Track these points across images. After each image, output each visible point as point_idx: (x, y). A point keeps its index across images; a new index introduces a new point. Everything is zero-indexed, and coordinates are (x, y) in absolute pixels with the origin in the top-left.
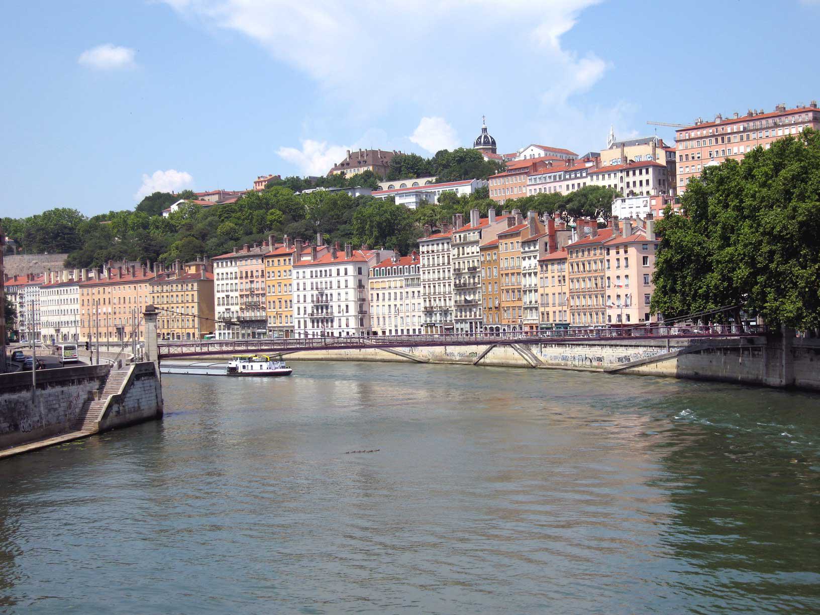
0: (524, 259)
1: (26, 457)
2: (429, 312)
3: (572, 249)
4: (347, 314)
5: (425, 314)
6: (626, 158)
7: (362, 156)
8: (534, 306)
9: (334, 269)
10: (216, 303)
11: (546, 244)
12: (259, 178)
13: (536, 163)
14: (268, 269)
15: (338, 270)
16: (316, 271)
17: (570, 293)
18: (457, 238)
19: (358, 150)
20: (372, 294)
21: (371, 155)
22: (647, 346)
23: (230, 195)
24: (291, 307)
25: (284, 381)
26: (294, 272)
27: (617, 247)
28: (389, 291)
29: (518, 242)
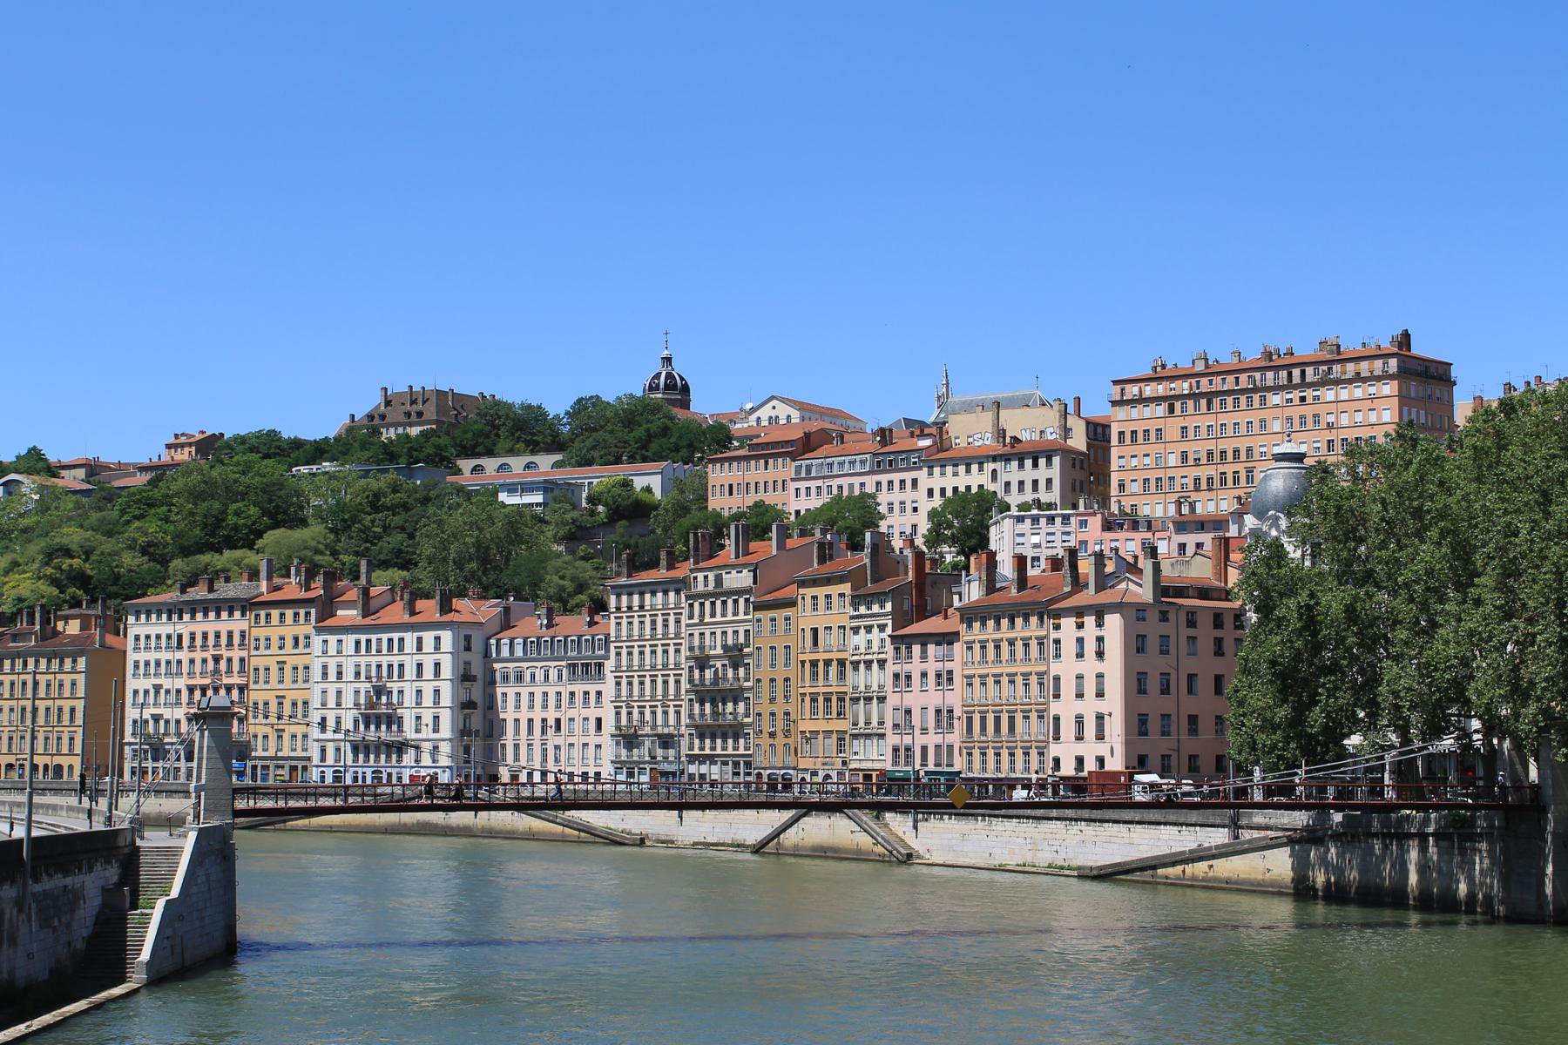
0: (856, 630)
1: (88, 1020)
2: (629, 739)
3: (970, 615)
4: (436, 736)
5: (618, 743)
6: (1004, 431)
7: (413, 402)
8: (875, 731)
9: (410, 638)
12: (176, 436)
13: (810, 433)
14: (256, 632)
15: (420, 640)
16: (379, 640)
17: (963, 706)
18: (703, 581)
20: (504, 695)
21: (434, 399)
22: (1182, 825)
23: (111, 469)
25: (747, 861)
26: (317, 641)
27: (1079, 612)
28: (531, 689)
29: (842, 595)
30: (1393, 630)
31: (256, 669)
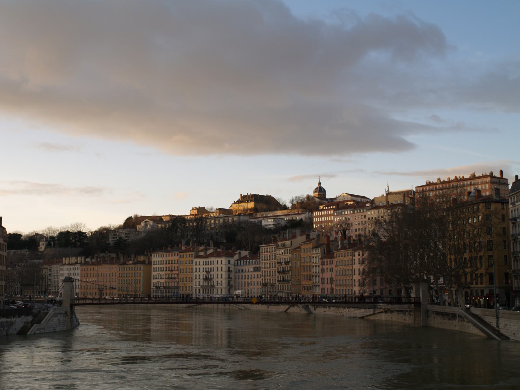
10: (152, 277)
11: (325, 250)
19: (246, 194)
24: (192, 281)
30: (310, 271)
31: (181, 269)
